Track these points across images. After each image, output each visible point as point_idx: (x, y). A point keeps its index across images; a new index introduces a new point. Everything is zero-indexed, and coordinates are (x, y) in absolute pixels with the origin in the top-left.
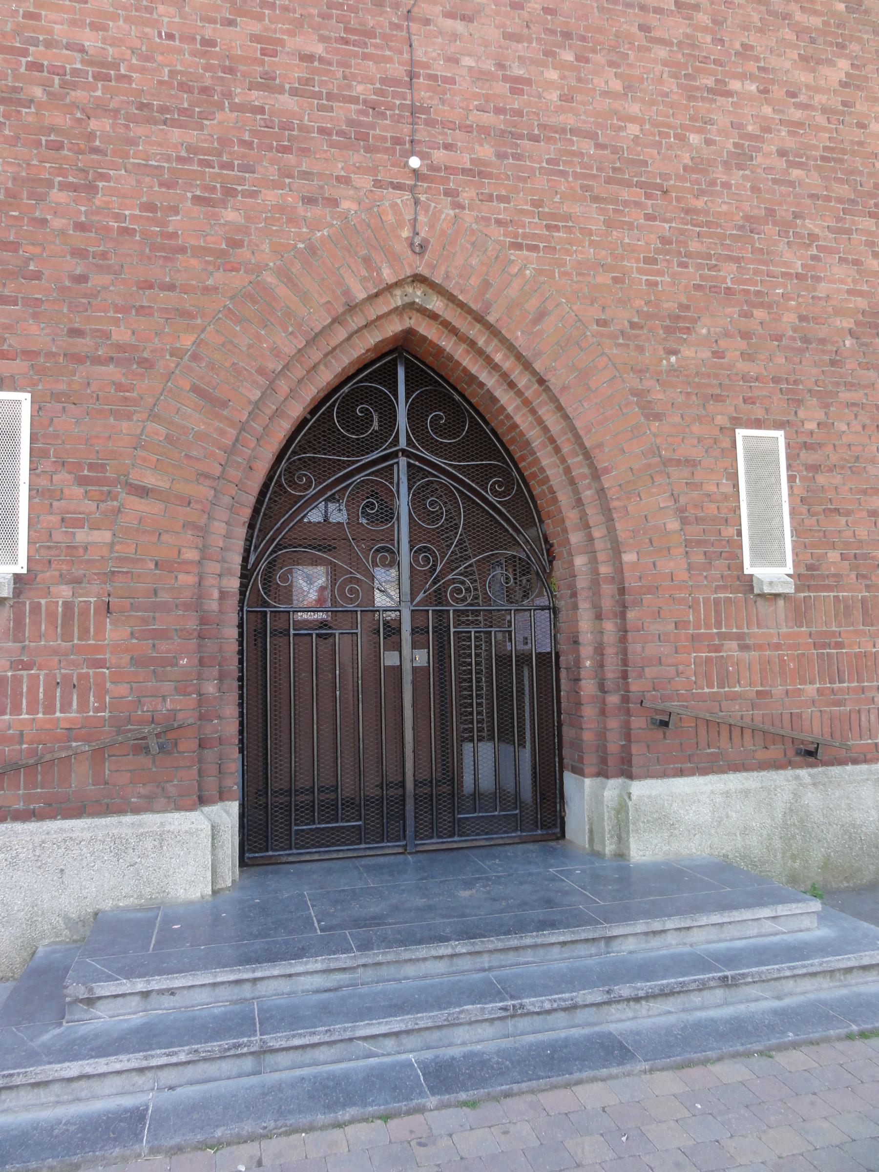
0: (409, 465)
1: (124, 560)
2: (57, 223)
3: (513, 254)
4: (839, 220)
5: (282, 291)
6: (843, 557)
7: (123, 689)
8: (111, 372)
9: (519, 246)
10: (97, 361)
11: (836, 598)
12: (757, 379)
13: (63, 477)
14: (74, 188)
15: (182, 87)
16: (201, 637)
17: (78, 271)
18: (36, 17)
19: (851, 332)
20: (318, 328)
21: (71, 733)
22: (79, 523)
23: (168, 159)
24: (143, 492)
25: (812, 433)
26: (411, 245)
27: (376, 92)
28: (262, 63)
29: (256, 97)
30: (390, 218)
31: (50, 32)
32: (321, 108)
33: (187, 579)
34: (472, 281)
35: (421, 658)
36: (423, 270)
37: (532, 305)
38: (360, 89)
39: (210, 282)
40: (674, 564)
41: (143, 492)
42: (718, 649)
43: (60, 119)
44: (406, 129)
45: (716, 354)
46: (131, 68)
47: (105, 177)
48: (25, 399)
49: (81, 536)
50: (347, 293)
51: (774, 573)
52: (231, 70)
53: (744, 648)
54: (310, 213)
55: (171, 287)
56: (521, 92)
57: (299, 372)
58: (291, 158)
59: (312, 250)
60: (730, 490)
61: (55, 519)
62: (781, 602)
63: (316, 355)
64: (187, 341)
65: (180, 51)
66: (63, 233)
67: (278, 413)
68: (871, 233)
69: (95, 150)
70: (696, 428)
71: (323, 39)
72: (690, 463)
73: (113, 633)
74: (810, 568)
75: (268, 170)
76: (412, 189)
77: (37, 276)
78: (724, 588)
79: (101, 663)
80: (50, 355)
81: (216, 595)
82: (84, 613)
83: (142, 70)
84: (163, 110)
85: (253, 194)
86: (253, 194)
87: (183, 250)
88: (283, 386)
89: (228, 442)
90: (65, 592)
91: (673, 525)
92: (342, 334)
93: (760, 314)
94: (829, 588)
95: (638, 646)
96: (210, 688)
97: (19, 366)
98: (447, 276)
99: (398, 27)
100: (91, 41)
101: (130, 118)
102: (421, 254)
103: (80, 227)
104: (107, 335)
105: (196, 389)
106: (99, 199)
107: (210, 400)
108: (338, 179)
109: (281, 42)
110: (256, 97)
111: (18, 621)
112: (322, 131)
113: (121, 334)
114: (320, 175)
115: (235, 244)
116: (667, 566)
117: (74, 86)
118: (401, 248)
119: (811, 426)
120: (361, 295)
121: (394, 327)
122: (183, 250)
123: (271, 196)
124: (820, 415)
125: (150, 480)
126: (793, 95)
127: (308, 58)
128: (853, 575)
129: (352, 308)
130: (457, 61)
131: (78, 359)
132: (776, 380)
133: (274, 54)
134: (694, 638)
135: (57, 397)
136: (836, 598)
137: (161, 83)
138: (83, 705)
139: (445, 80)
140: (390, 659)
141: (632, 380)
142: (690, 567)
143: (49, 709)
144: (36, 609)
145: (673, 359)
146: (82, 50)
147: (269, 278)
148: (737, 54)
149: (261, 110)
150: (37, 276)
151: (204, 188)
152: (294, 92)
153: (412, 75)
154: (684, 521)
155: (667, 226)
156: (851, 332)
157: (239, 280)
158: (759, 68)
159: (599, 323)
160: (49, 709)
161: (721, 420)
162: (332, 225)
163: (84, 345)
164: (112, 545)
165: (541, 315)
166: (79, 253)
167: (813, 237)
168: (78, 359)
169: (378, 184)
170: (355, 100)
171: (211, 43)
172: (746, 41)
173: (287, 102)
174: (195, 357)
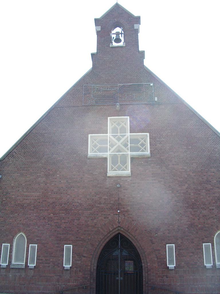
0: (120, 250)
1: (82, 265)
2: (75, 224)
3: (132, 222)
4: (185, 210)
5: (101, 230)
6: (185, 263)
7: (81, 281)
8: (81, 242)
9: (133, 221)
10: (79, 241)
11: (183, 270)
12: (170, 237)
13: (75, 255)
14: (77, 220)
15: (90, 205)
16: (91, 275)
17: (78, 230)
18: (74, 199)
19: (187, 228)
20: (105, 234)
21: (76, 286)
22: (77, 261)
23: (88, 215)
24: (84, 257)
25: (180, 244)
26: (118, 222)
27: (114, 202)
28: (99, 201)
29: (98, 205)
30: (115, 219)
31: (75, 201)
32: (107, 205)
33: (89, 267)
34: (127, 226)
35: (122, 278)
36: (120, 225)
37: (135, 229)
38: (112, 202)
39: (93, 230)
40: (156, 265)
41: (84, 257)
42: (162, 278)
43: (76, 212)
44: (118, 206)
45: (163, 233)
46: (84, 204)
47: (81, 218)
48: (72, 246)
49: (77, 262)
50: (109, 229)
51: (171, 266)
52: (95, 202)
53: (167, 277)
54: (105, 220)
55: (88, 231)
56: (134, 199)
57: (104, 240)
58: (103, 213)
59: (105, 224)
60: (165, 254)
61: (74, 260)
62: (173, 271)
63: (106, 237)
64: (90, 238)
65: (90, 201)
66: (76, 225)
67: (101, 245)
68: (191, 211)
69: (80, 215)
70: (160, 245)
71: (107, 196)
72: (159, 250)
73: (81, 274)
74: (179, 265)
75: (100, 215)
76: (118, 215)
77: (73, 231)
78: (164, 268)
79: (79, 278)
80: (74, 240)
81: (93, 269)
82: (77, 271)
83: (85, 204)
84: (87, 208)
85: (98, 218)
86: (98, 218)
87: (89, 226)
88: (102, 242)
89: (94, 250)
90: (75, 269)
91: (156, 259)
92: (109, 234)
93: (171, 227)
94: (182, 268)
95: (150, 277)
96: (92, 281)
97: (71, 242)
98: (123, 226)
99: (117, 193)
100: (79, 201)
101: (84, 210)
102: (120, 223)
103: (78, 224)
104: (80, 237)
105: (91, 244)
106: (80, 221)
107: (93, 245)
108: (109, 214)
109: (102, 197)
110: (98, 205)
111: (70, 272)
112: (107, 208)
113: (82, 237)
114: (106, 214)
115: (95, 225)
116: (155, 265)
117: (78, 207)
118: (117, 223)
119: (180, 243)
120: (111, 230)
121: (117, 232)
122: (89, 226)
123: (100, 218)
124: (181, 241)
125: (85, 255)
126: (178, 191)
127: (105, 199)
128: (186, 266)
129: (111, 231)
130: (125, 196)
131: (77, 241)
132: (174, 236)
133: (101, 199)
134: (159, 276)
135: (75, 245)
136: (183, 270)
137: (87, 205)
138: (77, 283)
139: (123, 199)
140: (117, 278)
141: (150, 238)
142: (158, 266)
143: (74, 283)
144: (72, 271)
145: (156, 235)
146: (78, 202)
147: (100, 229)
148: (168, 187)
149: (99, 207)
150: (73, 231)
151: (92, 218)
152: (103, 204)
153: (119, 199)
154: (158, 259)
155: (156, 215)
156: (187, 228)
157: (96, 229)
158: (172, 189)
159: (145, 230)
160: (74, 283)
161: (164, 243)
162: (108, 221)
163: (78, 239)
164: (81, 263)
165: (136, 230)
166: (77, 228)
167: (180, 213)
168: (77, 241)
169: (114, 215)
170: (111, 204)
171: (93, 199)
172: (170, 185)
173: (102, 205)
174: (90, 240)
